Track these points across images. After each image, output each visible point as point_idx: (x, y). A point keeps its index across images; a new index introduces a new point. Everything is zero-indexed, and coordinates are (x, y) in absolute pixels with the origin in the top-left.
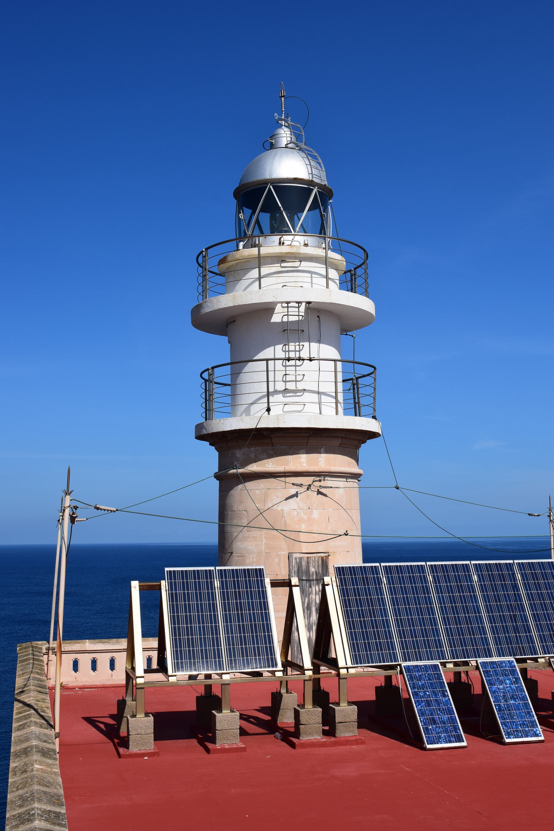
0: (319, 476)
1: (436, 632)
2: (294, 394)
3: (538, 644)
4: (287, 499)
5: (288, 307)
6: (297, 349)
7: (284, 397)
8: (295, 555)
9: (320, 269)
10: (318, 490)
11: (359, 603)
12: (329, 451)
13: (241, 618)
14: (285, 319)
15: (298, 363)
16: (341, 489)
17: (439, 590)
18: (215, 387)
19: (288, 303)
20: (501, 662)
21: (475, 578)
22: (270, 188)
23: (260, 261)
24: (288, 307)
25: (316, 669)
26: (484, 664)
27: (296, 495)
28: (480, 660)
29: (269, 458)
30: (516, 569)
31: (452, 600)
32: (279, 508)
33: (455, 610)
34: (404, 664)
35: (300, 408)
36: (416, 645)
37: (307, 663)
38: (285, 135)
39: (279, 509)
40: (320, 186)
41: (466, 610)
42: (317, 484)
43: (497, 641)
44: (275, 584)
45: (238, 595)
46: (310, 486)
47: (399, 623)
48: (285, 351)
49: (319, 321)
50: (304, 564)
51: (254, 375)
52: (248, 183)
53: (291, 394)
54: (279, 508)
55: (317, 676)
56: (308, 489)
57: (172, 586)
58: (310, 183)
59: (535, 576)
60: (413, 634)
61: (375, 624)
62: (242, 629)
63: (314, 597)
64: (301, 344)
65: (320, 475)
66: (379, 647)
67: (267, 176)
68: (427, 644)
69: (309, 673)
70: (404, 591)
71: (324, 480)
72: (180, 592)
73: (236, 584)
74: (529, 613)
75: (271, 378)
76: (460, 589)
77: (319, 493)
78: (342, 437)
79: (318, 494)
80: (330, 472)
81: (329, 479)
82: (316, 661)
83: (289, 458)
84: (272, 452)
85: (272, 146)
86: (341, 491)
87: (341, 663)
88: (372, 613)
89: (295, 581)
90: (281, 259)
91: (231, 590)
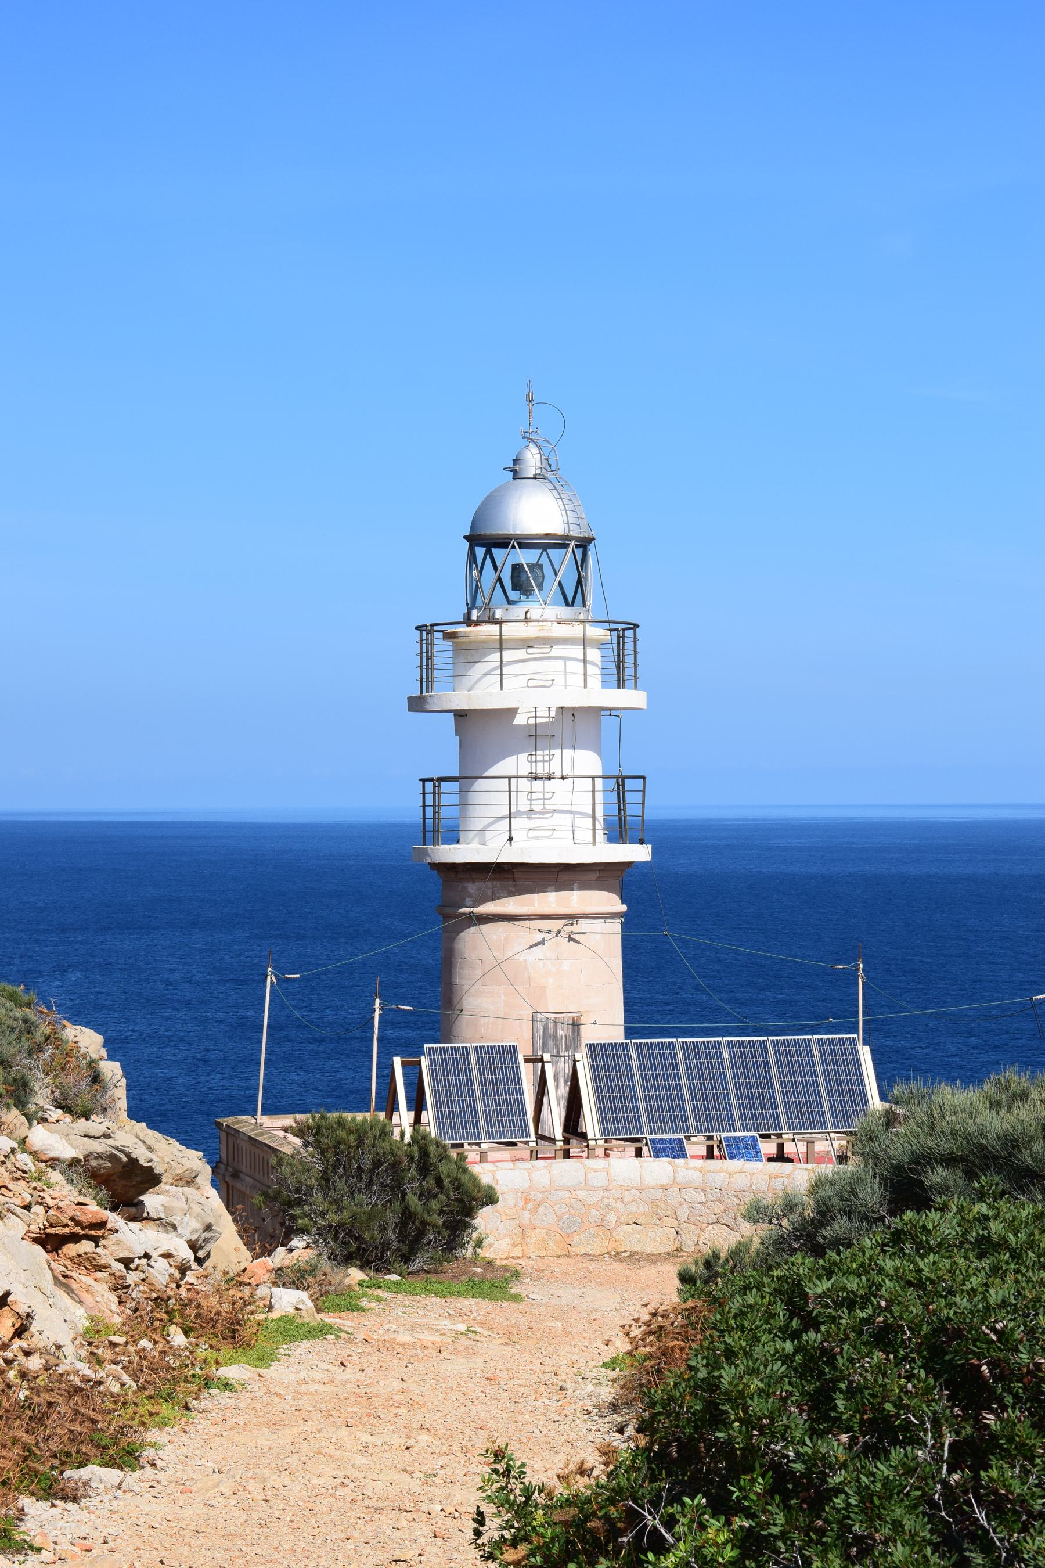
1: (683, 1107)
3: (783, 1120)
4: (531, 947)
6: (547, 758)
8: (539, 1016)
9: (577, 652)
11: (609, 1079)
13: (496, 1092)
14: (532, 721)
17: (688, 1067)
20: (745, 1137)
21: (726, 1055)
23: (501, 645)
25: (566, 1141)
26: (727, 1139)
27: (542, 942)
28: (723, 1135)
30: (769, 1046)
31: (701, 1077)
32: (521, 958)
33: (703, 1087)
34: (649, 1137)
35: (549, 833)
36: (662, 1120)
37: (559, 1135)
39: (521, 959)
41: (714, 1086)
42: (569, 928)
43: (743, 1117)
44: (527, 1060)
45: (493, 1071)
46: (559, 931)
47: (647, 1098)
48: (531, 762)
50: (551, 1025)
51: (489, 797)
52: (485, 535)
54: (521, 958)
55: (567, 1147)
56: (557, 935)
57: (432, 1062)
59: (788, 1053)
60: (660, 1109)
61: (623, 1100)
62: (497, 1103)
63: (562, 1065)
65: (572, 918)
66: (626, 1121)
68: (673, 1119)
69: (560, 1144)
70: (654, 1067)
72: (439, 1067)
73: (492, 1061)
74: (777, 1090)
75: (513, 801)
76: (710, 1065)
77: (570, 939)
82: (566, 1135)
84: (513, 889)
87: (590, 1136)
88: (656, 1077)
89: (547, 1057)
90: (527, 643)
91: (487, 1066)
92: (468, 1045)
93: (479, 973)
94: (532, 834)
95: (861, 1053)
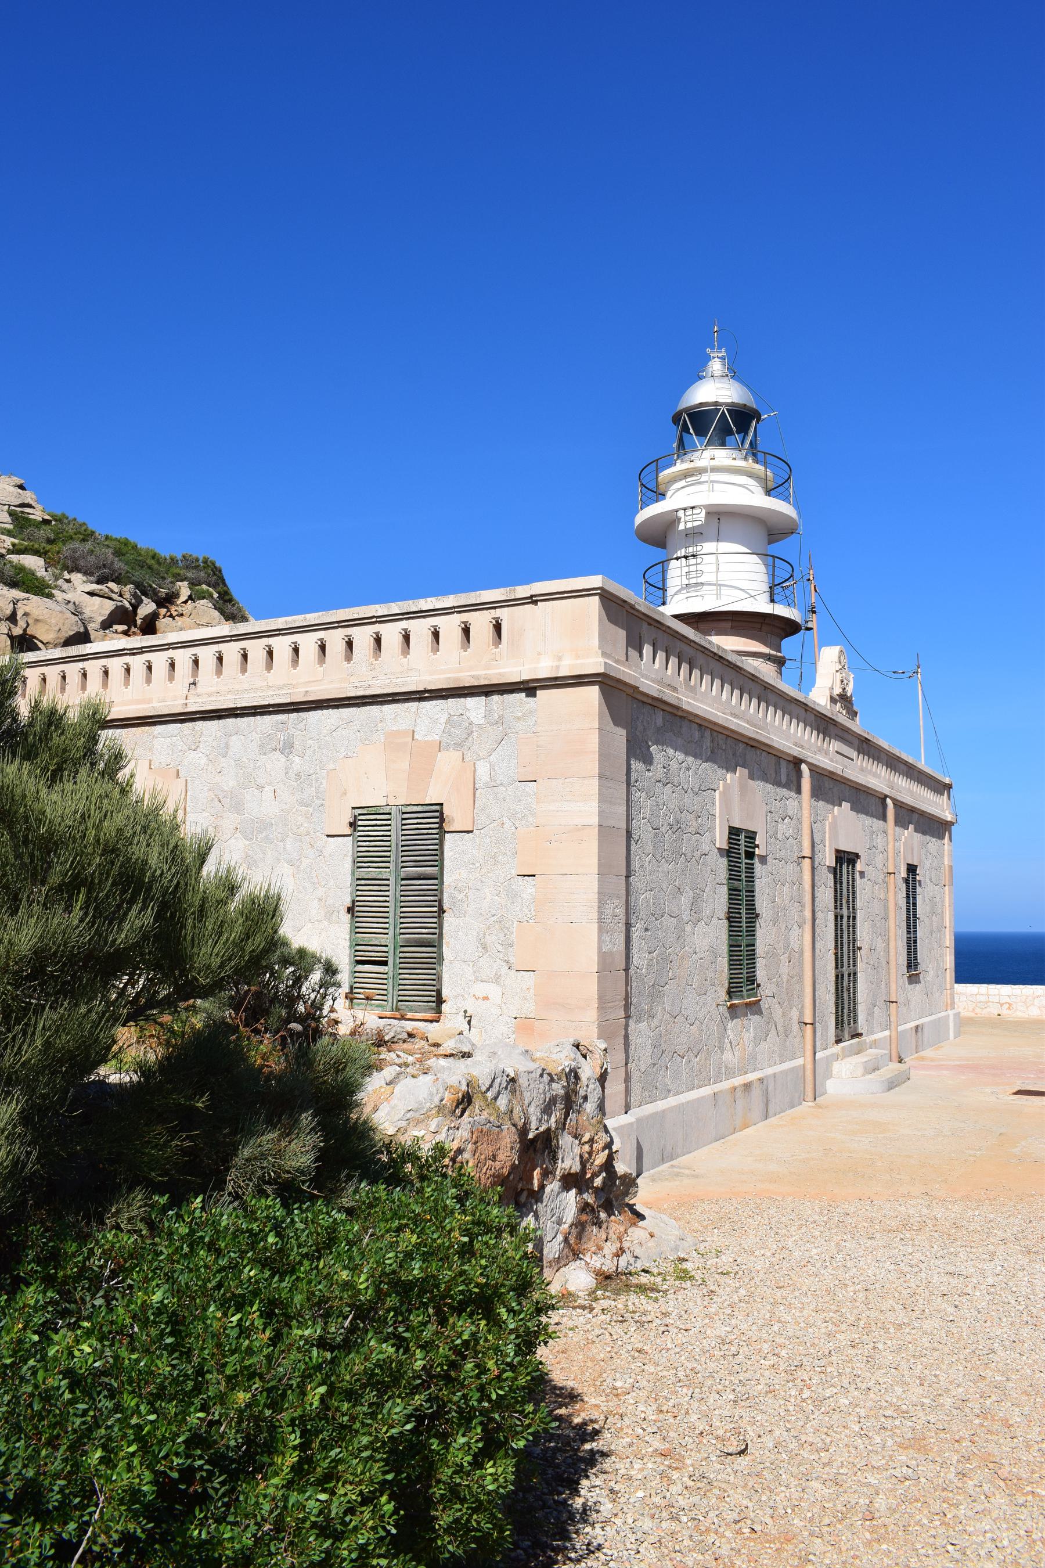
38: (716, 366)
40: (727, 404)
51: (676, 572)
58: (716, 404)
90: (686, 475)
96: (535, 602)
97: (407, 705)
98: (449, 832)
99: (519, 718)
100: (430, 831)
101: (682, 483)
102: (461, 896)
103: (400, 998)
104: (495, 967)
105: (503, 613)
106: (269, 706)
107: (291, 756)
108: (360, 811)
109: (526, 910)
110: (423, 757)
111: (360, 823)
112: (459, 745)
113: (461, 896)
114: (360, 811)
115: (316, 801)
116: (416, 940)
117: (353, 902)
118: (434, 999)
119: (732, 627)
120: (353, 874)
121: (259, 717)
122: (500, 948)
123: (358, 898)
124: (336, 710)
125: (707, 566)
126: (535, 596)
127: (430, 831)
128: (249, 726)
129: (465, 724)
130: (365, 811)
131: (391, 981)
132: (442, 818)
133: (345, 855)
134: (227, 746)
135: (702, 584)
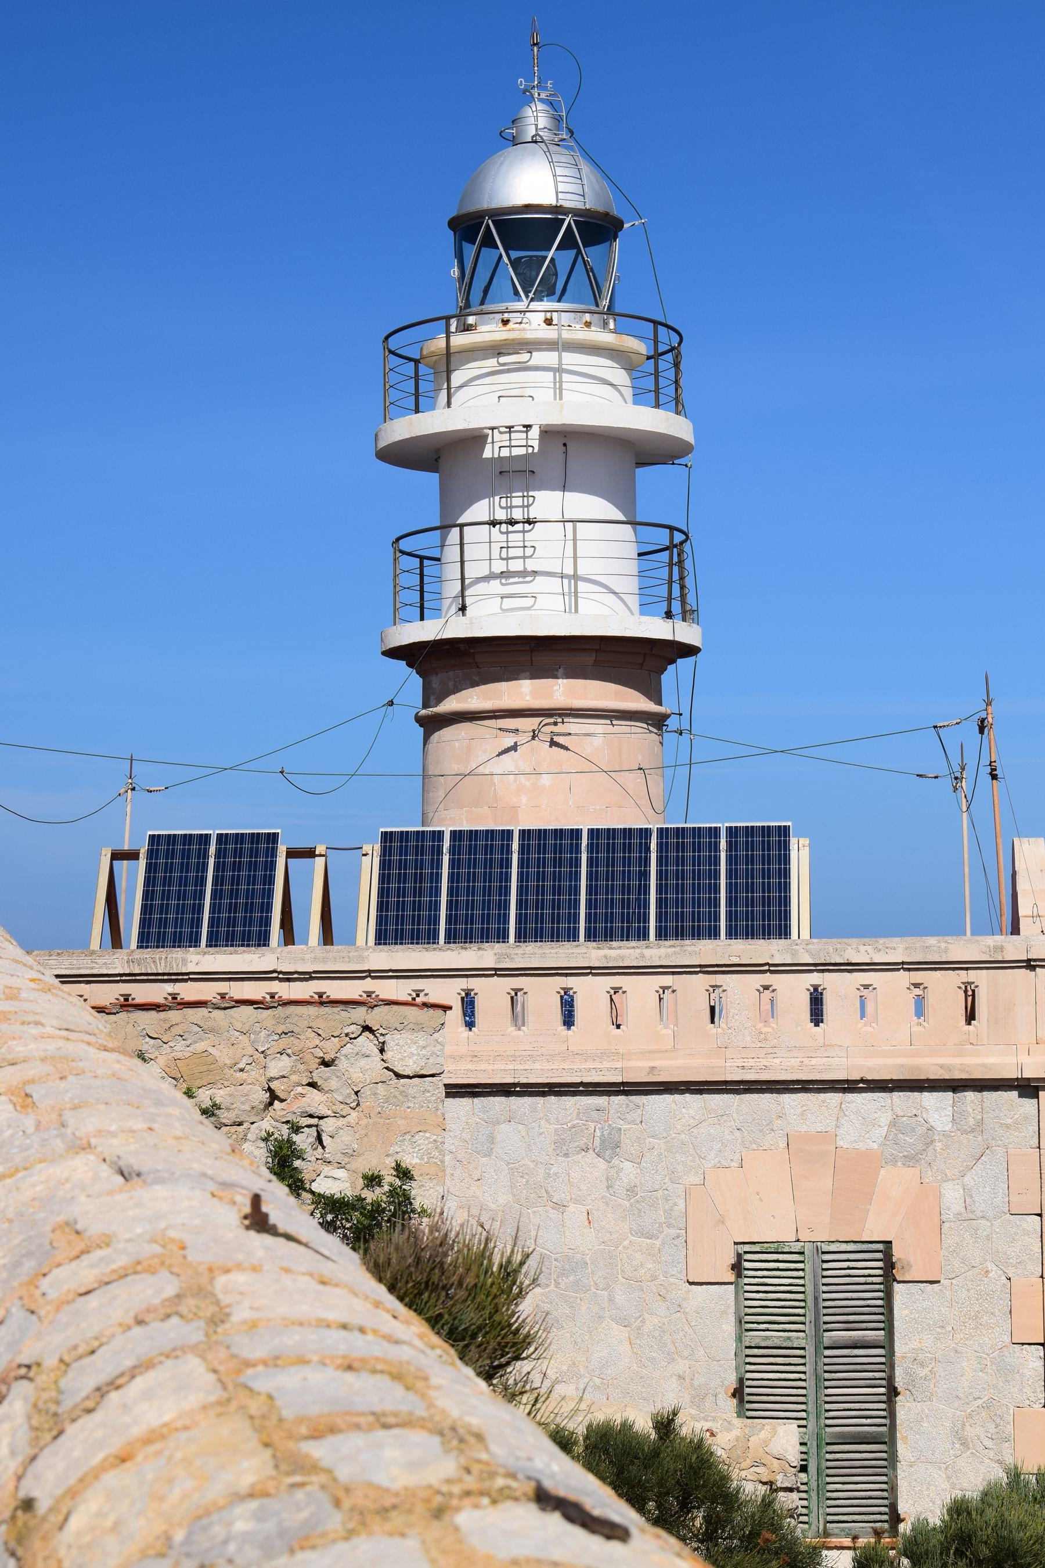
0: (551, 716)
2: (521, 580)
5: (510, 432)
7: (503, 584)
10: (552, 739)
11: (402, 878)
12: (573, 673)
14: (505, 453)
15: (527, 527)
16: (593, 739)
18: (419, 566)
19: (510, 427)
22: (488, 226)
24: (510, 432)
27: (514, 748)
29: (473, 687)
38: (536, 118)
40: (575, 212)
49: (566, 453)
51: (480, 546)
53: (516, 580)
56: (533, 738)
58: (557, 209)
64: (531, 493)
67: (485, 206)
71: (563, 723)
77: (553, 743)
78: (597, 650)
79: (551, 746)
80: (571, 709)
81: (572, 720)
83: (503, 686)
84: (476, 678)
85: (515, 141)
86: (598, 741)
90: (497, 350)
92: (211, 832)
93: (441, 793)
94: (508, 603)
95: (794, 854)
96: (1033, 968)
97: (822, 1096)
98: (899, 1282)
99: (1008, 1127)
100: (870, 1280)
101: (491, 363)
102: (923, 1372)
103: (830, 1518)
104: (983, 1470)
105: (980, 978)
106: (582, 1084)
107: (615, 1161)
108: (747, 1248)
109: (1028, 1390)
110: (856, 1174)
111: (747, 1265)
112: (911, 1160)
113: (923, 1372)
114: (747, 1248)
115: (667, 1230)
116: (842, 1435)
117: (741, 1381)
118: (886, 1517)
119: (596, 663)
120: (739, 1339)
121: (552, 1099)
122: (988, 1443)
123: (749, 1375)
124: (699, 1096)
125: (547, 546)
126: (1035, 960)
127: (870, 1280)
128: (534, 1110)
129: (921, 1130)
130: (757, 1248)
131: (814, 1495)
132: (889, 1264)
133: (724, 1312)
134: (491, 1139)
135: (535, 573)
